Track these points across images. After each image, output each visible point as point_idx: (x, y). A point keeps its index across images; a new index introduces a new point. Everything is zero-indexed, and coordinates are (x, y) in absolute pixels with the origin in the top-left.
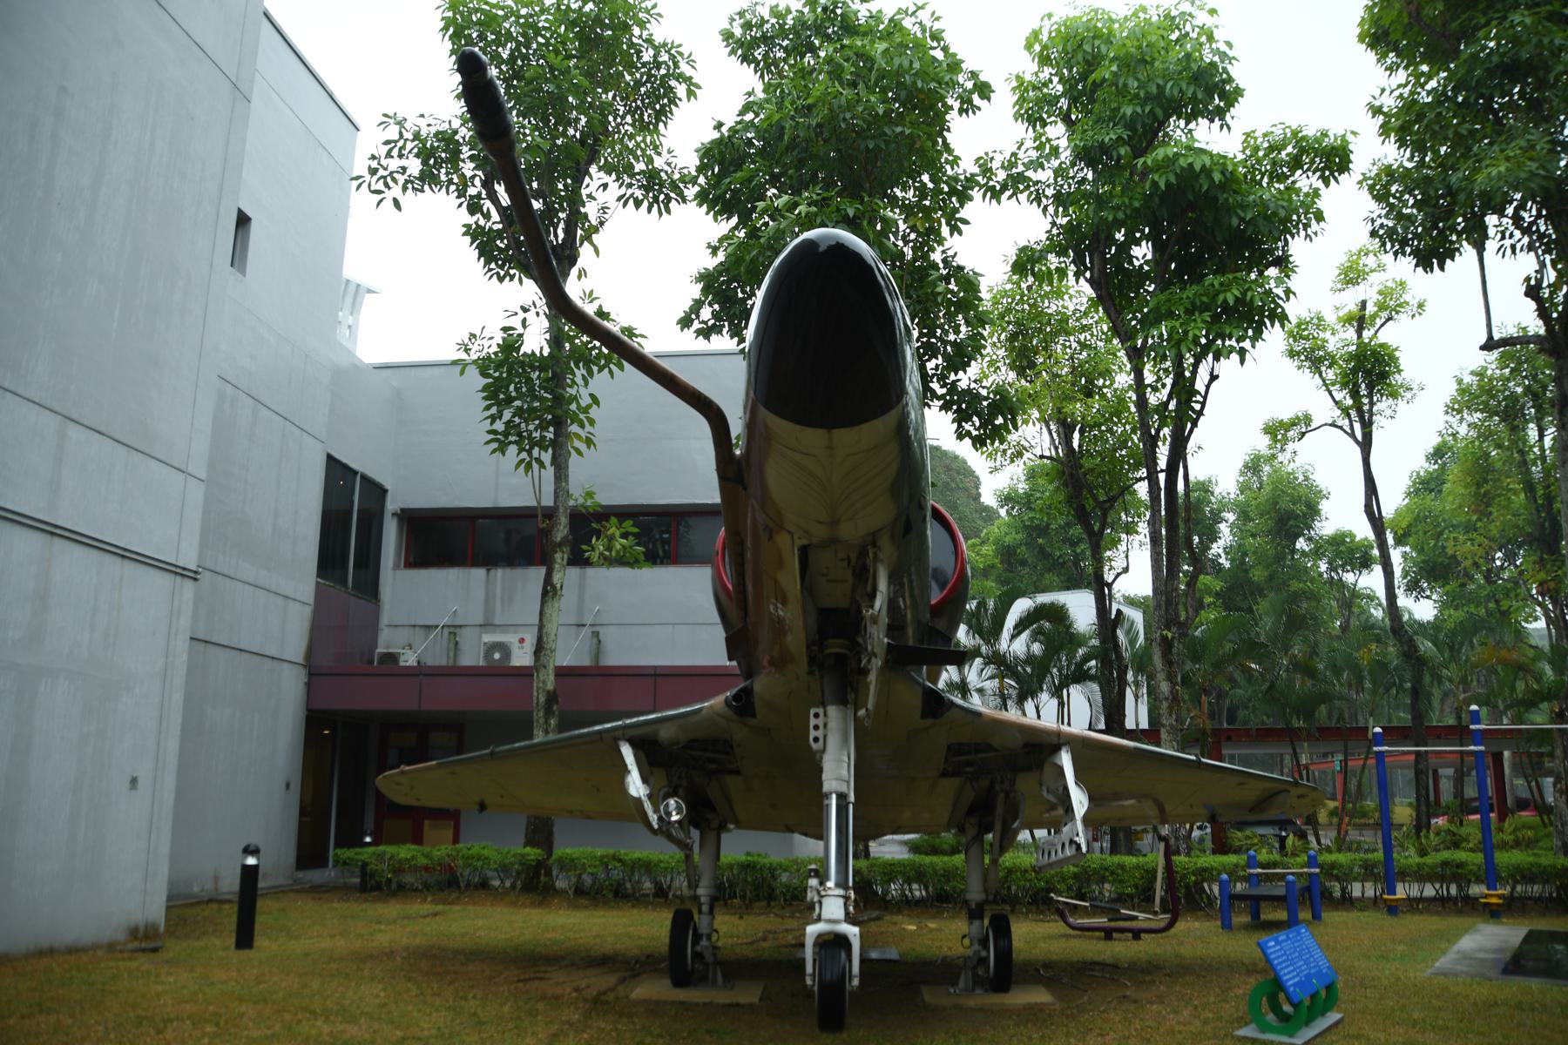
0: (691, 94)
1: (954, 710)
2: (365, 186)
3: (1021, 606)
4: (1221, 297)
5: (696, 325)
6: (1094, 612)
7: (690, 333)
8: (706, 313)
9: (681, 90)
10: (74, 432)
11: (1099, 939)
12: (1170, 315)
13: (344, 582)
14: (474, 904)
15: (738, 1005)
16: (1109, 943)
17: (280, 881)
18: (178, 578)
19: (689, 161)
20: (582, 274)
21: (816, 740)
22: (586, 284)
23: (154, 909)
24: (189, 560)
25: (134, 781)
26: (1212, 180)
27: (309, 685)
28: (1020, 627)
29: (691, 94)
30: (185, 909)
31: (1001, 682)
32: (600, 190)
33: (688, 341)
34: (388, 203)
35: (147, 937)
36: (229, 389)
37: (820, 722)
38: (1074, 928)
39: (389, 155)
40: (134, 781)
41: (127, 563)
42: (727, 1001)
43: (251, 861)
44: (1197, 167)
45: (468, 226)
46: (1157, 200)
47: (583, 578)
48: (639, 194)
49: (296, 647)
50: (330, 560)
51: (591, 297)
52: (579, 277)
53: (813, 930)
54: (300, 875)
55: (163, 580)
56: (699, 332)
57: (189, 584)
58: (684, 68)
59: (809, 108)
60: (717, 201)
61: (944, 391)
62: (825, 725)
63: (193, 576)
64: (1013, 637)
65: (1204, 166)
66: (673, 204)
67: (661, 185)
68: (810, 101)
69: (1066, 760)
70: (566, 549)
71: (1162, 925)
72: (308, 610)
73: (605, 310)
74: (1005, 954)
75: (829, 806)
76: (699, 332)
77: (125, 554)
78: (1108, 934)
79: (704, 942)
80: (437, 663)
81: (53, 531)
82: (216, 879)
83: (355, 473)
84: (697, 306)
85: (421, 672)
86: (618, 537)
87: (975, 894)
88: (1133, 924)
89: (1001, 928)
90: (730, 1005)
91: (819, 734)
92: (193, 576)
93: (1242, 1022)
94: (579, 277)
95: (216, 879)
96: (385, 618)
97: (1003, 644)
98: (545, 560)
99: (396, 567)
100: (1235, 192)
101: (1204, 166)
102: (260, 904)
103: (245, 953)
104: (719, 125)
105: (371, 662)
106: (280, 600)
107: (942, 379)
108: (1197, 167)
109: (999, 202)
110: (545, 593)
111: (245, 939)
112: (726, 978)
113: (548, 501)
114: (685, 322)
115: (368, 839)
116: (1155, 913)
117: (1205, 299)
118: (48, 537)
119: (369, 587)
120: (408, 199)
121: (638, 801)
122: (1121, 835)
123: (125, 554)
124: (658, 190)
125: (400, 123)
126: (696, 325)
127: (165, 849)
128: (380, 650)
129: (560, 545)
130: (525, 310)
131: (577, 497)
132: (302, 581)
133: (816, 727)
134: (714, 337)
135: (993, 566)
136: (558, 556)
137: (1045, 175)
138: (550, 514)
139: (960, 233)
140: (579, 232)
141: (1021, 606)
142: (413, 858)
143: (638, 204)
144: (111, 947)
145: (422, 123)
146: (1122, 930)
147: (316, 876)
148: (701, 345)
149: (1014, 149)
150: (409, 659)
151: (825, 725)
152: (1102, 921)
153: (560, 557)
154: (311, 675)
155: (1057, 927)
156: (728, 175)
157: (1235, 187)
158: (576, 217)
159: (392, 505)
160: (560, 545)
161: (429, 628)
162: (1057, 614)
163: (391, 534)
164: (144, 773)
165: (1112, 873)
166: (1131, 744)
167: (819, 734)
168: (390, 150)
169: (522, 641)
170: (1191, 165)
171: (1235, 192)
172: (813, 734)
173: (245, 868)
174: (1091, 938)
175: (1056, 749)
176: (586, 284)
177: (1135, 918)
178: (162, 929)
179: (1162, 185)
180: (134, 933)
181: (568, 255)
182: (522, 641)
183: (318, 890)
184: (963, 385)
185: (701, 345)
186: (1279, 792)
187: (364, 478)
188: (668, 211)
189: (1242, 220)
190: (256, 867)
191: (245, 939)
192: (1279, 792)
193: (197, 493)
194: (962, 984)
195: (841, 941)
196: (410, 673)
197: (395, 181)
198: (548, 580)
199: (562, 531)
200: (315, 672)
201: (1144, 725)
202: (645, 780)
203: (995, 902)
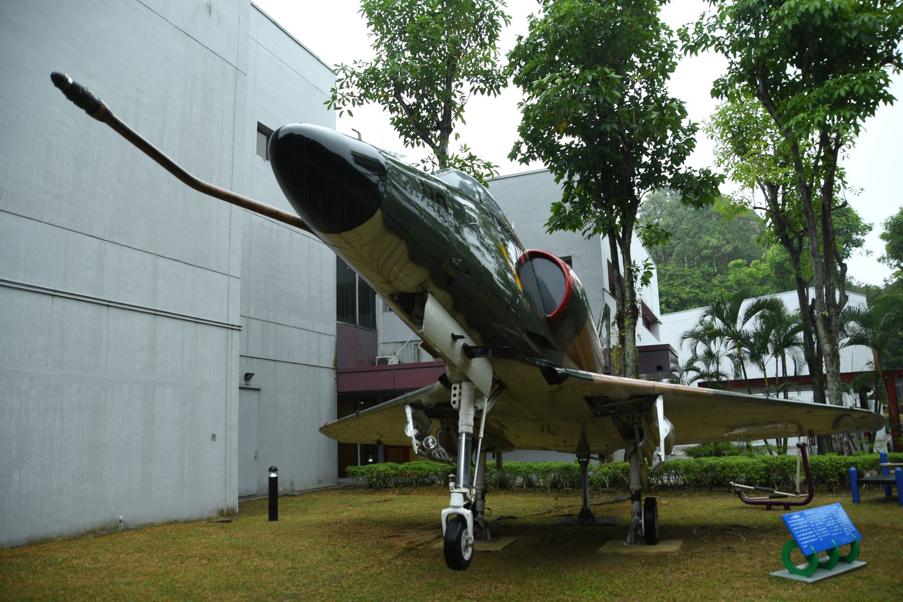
0: (507, 22)
1: (569, 378)
2: (332, 106)
3: (746, 304)
4: (836, 93)
5: (519, 156)
6: (798, 302)
7: (516, 162)
8: (524, 149)
9: (501, 21)
10: (162, 262)
11: (763, 509)
12: (804, 110)
13: (354, 322)
14: (419, 494)
15: (489, 551)
16: (770, 512)
17: (330, 484)
18: (230, 331)
19: (503, 62)
20: (457, 136)
21: (454, 402)
22: (461, 142)
23: (233, 502)
24: (235, 320)
25: (214, 436)
26: (823, 16)
27: (337, 379)
28: (748, 316)
29: (507, 22)
30: (246, 501)
31: (739, 350)
32: (464, 89)
33: (516, 168)
34: (346, 113)
35: (228, 515)
37: (457, 392)
38: (747, 503)
39: (341, 87)
40: (214, 436)
41: (199, 326)
42: (484, 549)
43: (273, 475)
44: (812, 10)
45: (393, 119)
46: (789, 36)
48: (482, 85)
49: (327, 356)
50: (344, 310)
51: (465, 148)
52: (456, 138)
53: (445, 512)
54: (341, 480)
55: (223, 332)
56: (522, 161)
57: (236, 333)
58: (501, 8)
59: (563, 17)
60: (524, 81)
61: (671, 176)
62: (460, 394)
63: (238, 329)
64: (744, 323)
65: (816, 9)
66: (501, 89)
67: (494, 78)
68: (562, 14)
69: (659, 404)
71: (803, 500)
72: (333, 339)
73: (473, 154)
74: (650, 523)
75: (461, 440)
76: (522, 161)
77: (197, 321)
78: (769, 506)
79: (479, 516)
80: (410, 362)
81: (156, 313)
82: (292, 484)
84: (517, 148)
85: (401, 367)
87: (635, 486)
88: (783, 500)
89: (651, 506)
90: (484, 552)
91: (456, 399)
92: (238, 329)
93: (780, 567)
94: (456, 138)
95: (292, 484)
96: (381, 340)
97: (738, 327)
99: (385, 310)
100: (845, 20)
101: (816, 9)
102: (279, 500)
103: (274, 522)
104: (520, 38)
105: (374, 364)
106: (315, 335)
107: (670, 169)
108: (812, 10)
109: (697, 54)
111: (273, 516)
112: (493, 536)
114: (513, 156)
115: (371, 460)
116: (797, 493)
117: (826, 96)
118: (153, 317)
119: (370, 323)
120: (356, 110)
121: (410, 438)
122: (825, 441)
123: (197, 321)
124: (492, 83)
125: (344, 69)
126: (519, 156)
127: (235, 469)
128: (379, 357)
130: (423, 161)
132: (328, 322)
133: (455, 395)
134: (531, 162)
135: (768, 276)
137: (721, 33)
139: (669, 78)
140: (453, 113)
141: (746, 304)
142: (386, 470)
143: (483, 91)
144: (209, 520)
145: (355, 67)
146: (778, 504)
147: (348, 481)
148: (524, 169)
149: (697, 20)
150: (393, 361)
151: (460, 394)
152: (765, 498)
154: (338, 373)
156: (531, 64)
157: (845, 17)
158: (450, 105)
161: (404, 342)
162: (776, 307)
164: (219, 431)
165: (789, 467)
167: (456, 399)
168: (342, 85)
170: (807, 9)
171: (845, 20)
172: (453, 399)
173: (271, 479)
174: (758, 509)
175: (655, 397)
176: (461, 142)
177: (787, 496)
178: (237, 510)
179: (790, 27)
180: (221, 513)
181: (446, 128)
183: (354, 488)
184: (681, 172)
185: (524, 169)
186: (843, 416)
188: (499, 93)
189: (849, 39)
190: (276, 478)
191: (273, 516)
192: (843, 416)
193: (236, 285)
194: (628, 540)
195: (461, 518)
196: (394, 368)
197: (348, 100)
200: (340, 371)
201: (806, 371)
202: (415, 427)
203: (649, 491)
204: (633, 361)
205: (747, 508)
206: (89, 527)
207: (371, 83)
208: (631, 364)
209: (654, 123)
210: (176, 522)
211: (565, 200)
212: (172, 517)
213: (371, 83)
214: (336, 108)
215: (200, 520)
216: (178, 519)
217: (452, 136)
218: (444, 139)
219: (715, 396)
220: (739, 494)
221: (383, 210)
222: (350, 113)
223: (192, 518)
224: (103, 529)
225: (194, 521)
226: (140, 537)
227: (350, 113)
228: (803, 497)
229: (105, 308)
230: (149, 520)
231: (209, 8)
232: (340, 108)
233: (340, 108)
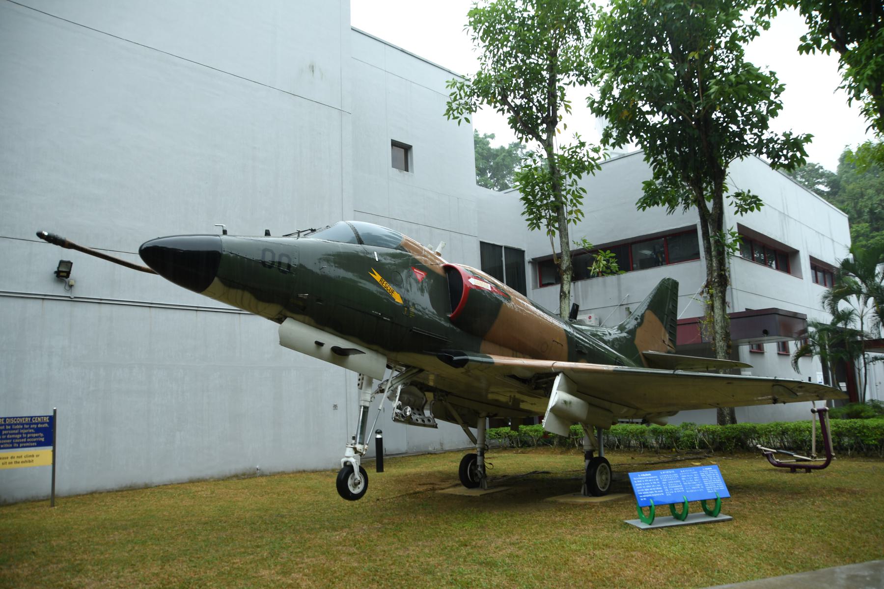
2: (452, 117)
10: (453, 234)
11: (787, 472)
25: (335, 406)
36: (414, 226)
38: (775, 465)
40: (335, 406)
43: (379, 436)
47: (619, 280)
70: (570, 273)
71: (822, 463)
78: (793, 469)
82: (441, 444)
83: (501, 247)
86: (602, 260)
88: (807, 463)
95: (441, 444)
98: (559, 280)
99: (535, 287)
110: (561, 296)
113: (558, 250)
114: (605, 141)
126: (612, 141)
129: (565, 271)
131: (573, 247)
136: (565, 277)
138: (559, 256)
146: (801, 467)
153: (566, 277)
155: (765, 464)
159: (528, 258)
160: (565, 271)
163: (529, 271)
164: (341, 403)
166: (611, 367)
169: (590, 318)
175: (557, 374)
182: (590, 318)
187: (506, 248)
194: (582, 491)
198: (562, 291)
199: (566, 263)
204: (722, 328)
205: (775, 470)
206: (233, 472)
207: (487, 89)
208: (719, 331)
209: (712, 97)
210: (304, 471)
211: (657, 177)
212: (301, 468)
213: (487, 89)
214: (455, 118)
215: (325, 471)
216: (306, 469)
217: (560, 126)
218: (551, 131)
219: (615, 372)
220: (768, 456)
221: (219, 277)
222: (467, 120)
223: (318, 469)
224: (244, 474)
225: (320, 471)
226: (263, 480)
227: (467, 120)
228: (821, 461)
229: (237, 316)
230: (281, 469)
231: (312, 68)
232: (457, 118)
233: (457, 118)
